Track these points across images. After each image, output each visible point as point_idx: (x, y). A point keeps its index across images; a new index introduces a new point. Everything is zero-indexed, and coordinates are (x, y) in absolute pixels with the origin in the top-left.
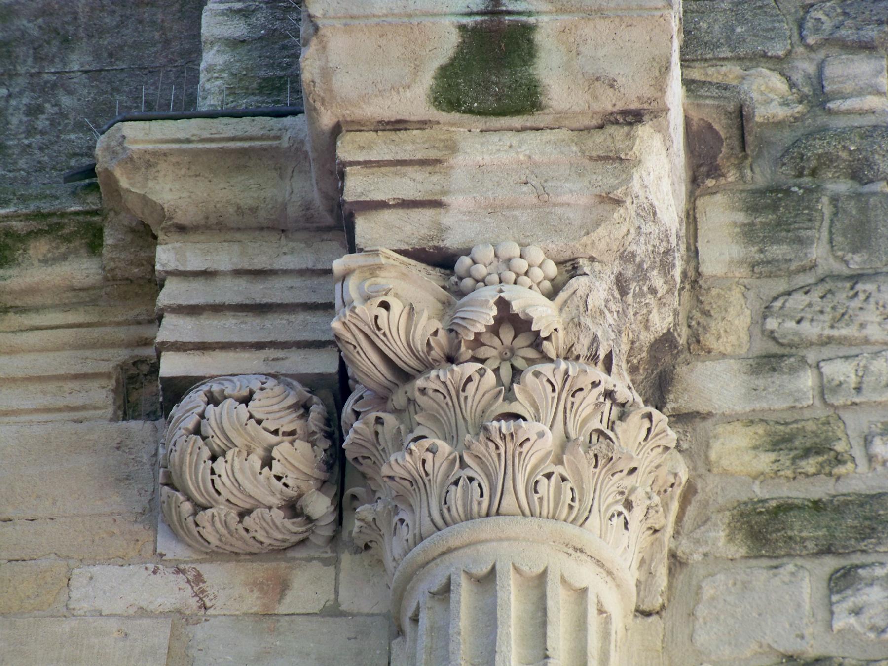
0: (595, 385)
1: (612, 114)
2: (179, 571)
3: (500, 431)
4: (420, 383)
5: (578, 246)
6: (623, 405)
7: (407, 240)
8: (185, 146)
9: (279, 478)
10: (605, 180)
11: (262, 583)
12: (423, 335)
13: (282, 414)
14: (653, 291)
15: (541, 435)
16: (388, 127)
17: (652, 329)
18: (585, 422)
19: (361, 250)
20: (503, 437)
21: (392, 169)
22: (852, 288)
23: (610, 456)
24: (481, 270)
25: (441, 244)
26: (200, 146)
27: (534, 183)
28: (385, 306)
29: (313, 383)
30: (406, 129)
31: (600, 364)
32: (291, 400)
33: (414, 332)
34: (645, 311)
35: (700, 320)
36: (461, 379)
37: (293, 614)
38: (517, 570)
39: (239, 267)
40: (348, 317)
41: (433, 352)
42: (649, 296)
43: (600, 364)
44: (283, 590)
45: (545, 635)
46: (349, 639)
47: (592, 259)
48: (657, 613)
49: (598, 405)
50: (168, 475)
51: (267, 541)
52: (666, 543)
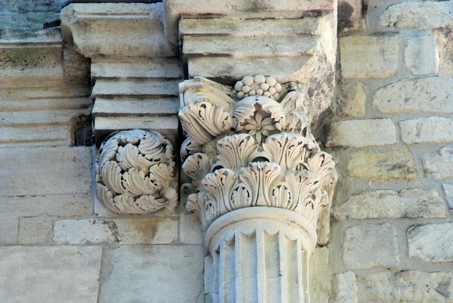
0: (300, 143)
1: (307, 11)
2: (105, 223)
3: (257, 167)
4: (220, 142)
5: (293, 76)
6: (311, 150)
7: (212, 73)
8: (104, 17)
9: (153, 181)
10: (304, 45)
11: (144, 229)
12: (221, 119)
13: (154, 151)
14: (323, 92)
15: (276, 168)
16: (203, 17)
17: (322, 108)
18: (295, 160)
19: (192, 78)
20: (259, 170)
21: (205, 37)
22: (414, 85)
23: (307, 177)
24: (247, 89)
25: (228, 75)
26: (111, 17)
27: (271, 46)
28: (204, 106)
29: (165, 134)
30: (211, 18)
31: (301, 132)
32: (157, 144)
33: (217, 117)
34: (319, 101)
35: (343, 100)
36: (239, 141)
37: (159, 244)
38: (266, 232)
39: (130, 76)
40: (187, 111)
41: (225, 127)
42: (322, 94)
43: (301, 132)
44: (154, 232)
45: (279, 264)
46: (185, 257)
47: (298, 83)
48: (326, 245)
49: (301, 152)
50: (101, 178)
51: (146, 209)
52: (329, 210)
